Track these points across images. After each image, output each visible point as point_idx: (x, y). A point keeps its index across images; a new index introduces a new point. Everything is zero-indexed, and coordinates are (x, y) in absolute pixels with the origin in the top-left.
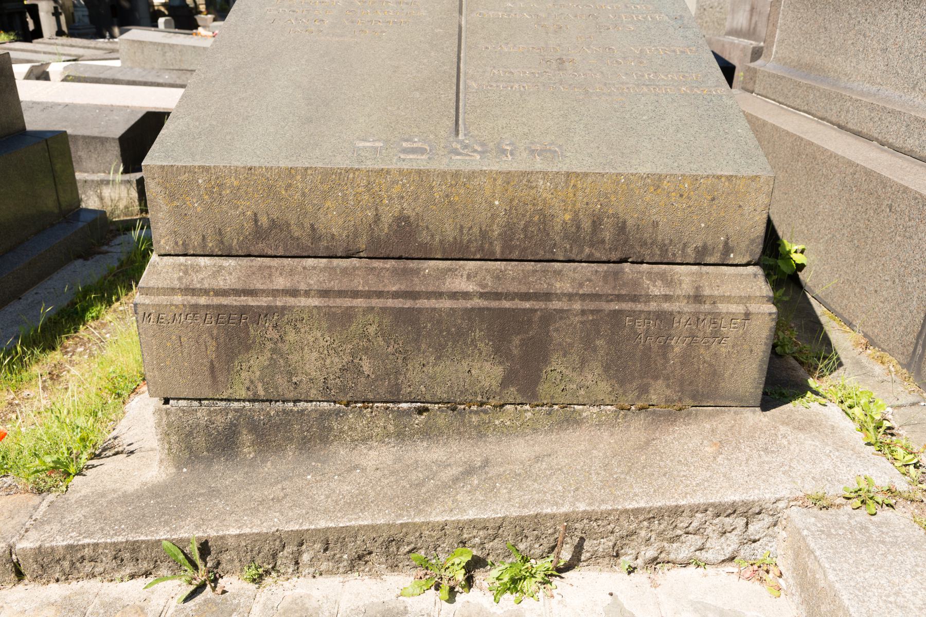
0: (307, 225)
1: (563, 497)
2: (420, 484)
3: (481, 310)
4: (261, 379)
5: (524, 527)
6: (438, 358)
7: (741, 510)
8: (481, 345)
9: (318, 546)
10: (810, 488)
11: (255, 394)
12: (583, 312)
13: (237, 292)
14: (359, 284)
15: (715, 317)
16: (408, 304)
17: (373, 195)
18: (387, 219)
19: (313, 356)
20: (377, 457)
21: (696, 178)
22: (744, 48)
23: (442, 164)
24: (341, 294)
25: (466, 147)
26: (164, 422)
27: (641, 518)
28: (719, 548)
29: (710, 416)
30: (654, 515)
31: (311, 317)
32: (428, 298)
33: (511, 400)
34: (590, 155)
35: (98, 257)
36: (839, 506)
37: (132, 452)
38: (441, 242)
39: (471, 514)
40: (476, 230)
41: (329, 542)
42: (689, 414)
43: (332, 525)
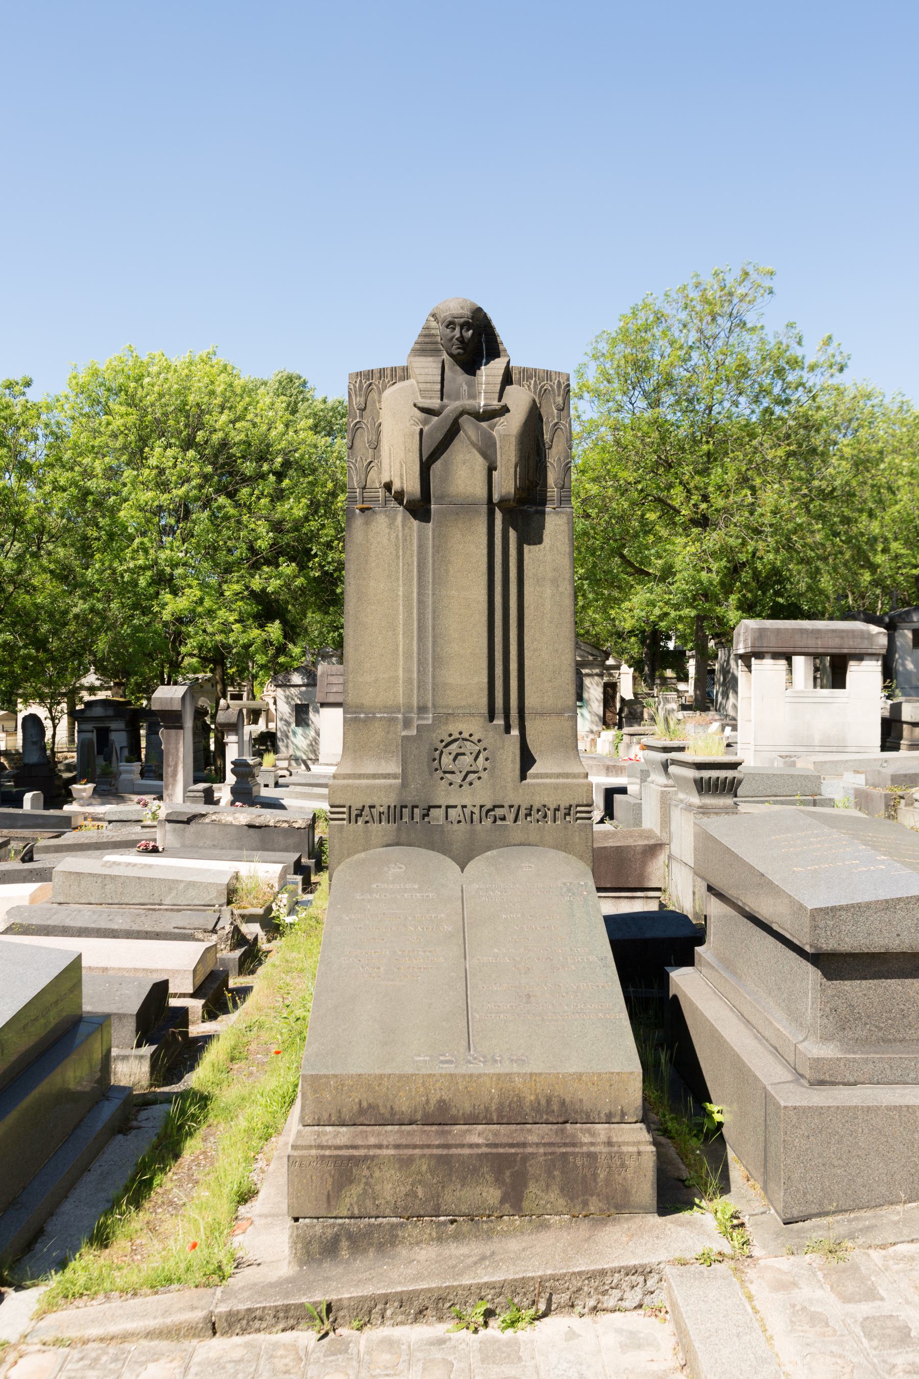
0: (389, 1106)
1: (538, 1268)
2: (454, 1267)
3: (487, 1154)
4: (357, 1202)
5: (517, 1287)
6: (463, 1186)
7: (640, 1270)
8: (487, 1176)
9: (396, 1304)
10: (678, 1255)
11: (352, 1213)
12: (545, 1154)
13: (347, 1147)
14: (417, 1140)
15: (621, 1155)
16: (445, 1152)
17: (426, 1088)
18: (433, 1101)
19: (390, 1186)
20: (426, 1253)
21: (600, 1074)
23: (463, 1069)
24: (407, 1146)
25: (475, 1059)
26: (294, 1234)
27: (584, 1278)
29: (627, 1219)
31: (389, 1161)
32: (456, 1148)
33: (507, 1213)
34: (543, 1062)
35: (134, 1132)
36: (692, 1264)
37: (259, 1264)
38: (463, 1114)
39: (486, 1279)
40: (482, 1107)
41: (403, 1300)
42: (614, 1219)
43: (405, 1289)
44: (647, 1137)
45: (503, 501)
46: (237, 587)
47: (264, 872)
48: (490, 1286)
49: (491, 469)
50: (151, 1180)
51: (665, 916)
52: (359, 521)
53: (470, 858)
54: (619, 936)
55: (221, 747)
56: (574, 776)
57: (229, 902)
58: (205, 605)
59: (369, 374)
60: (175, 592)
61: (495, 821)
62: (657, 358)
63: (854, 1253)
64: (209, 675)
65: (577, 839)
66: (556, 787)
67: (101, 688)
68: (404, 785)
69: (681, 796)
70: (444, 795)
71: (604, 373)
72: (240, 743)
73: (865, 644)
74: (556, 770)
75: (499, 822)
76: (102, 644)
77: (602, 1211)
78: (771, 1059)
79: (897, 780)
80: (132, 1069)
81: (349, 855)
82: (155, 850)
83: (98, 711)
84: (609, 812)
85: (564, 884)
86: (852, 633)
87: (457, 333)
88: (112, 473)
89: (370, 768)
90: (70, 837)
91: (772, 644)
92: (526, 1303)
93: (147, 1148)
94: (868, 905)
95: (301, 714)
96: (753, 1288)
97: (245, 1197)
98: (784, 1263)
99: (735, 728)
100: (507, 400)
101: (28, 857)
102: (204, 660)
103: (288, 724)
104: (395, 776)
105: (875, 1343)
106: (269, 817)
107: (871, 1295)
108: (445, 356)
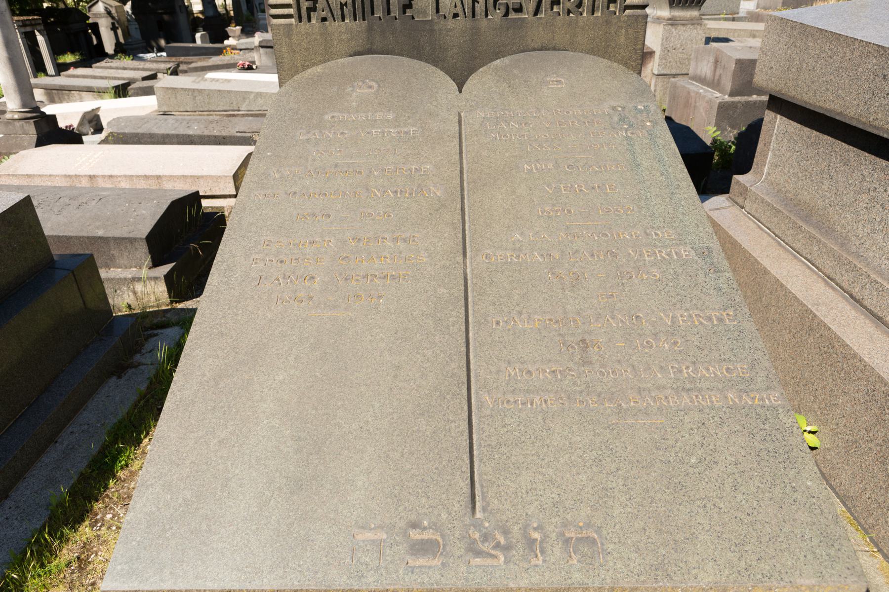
22: (710, 102)
35: (130, 371)
53: (472, 71)
61: (506, 14)
65: (622, 39)
75: (513, 15)
81: (304, 69)
82: (250, 68)
85: (614, 108)
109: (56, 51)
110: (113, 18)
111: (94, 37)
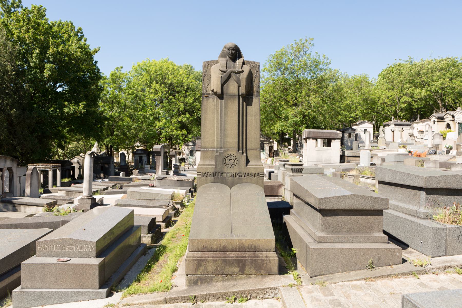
5: (243, 292)
10: (283, 285)
13: (200, 257)
14: (218, 256)
15: (269, 260)
18: (222, 246)
19: (211, 267)
20: (220, 284)
23: (230, 238)
24: (215, 257)
28: (272, 295)
30: (261, 290)
41: (214, 295)
44: (276, 255)
45: (242, 95)
46: (175, 120)
47: (181, 192)
48: (236, 292)
49: (239, 86)
50: (151, 266)
51: (283, 203)
52: (205, 100)
54: (271, 207)
55: (171, 161)
56: (260, 165)
57: (172, 199)
58: (166, 125)
59: (208, 62)
60: (159, 121)
62: (285, 62)
63: (328, 285)
64: (168, 143)
66: (255, 168)
67: (140, 146)
68: (216, 167)
69: (288, 173)
70: (226, 170)
71: (271, 66)
72: (176, 160)
73: (336, 136)
74: (255, 164)
76: (141, 135)
77: (264, 274)
78: (308, 236)
79: (343, 170)
80: (147, 239)
82: (153, 186)
83: (139, 152)
84: (270, 178)
86: (333, 133)
87: (231, 52)
88: (143, 90)
89: (207, 163)
90: (132, 183)
91: (312, 136)
92: (245, 296)
93: (150, 259)
94: (333, 197)
95: (191, 153)
96: (302, 293)
97: (175, 270)
98: (310, 287)
99: (302, 158)
100: (243, 69)
101: (121, 188)
102: (167, 139)
103: (188, 155)
104: (214, 165)
105: (332, 306)
106: (182, 178)
107: (332, 294)
108: (228, 57)
109: (63, 177)
110: (79, 164)
111: (72, 172)
